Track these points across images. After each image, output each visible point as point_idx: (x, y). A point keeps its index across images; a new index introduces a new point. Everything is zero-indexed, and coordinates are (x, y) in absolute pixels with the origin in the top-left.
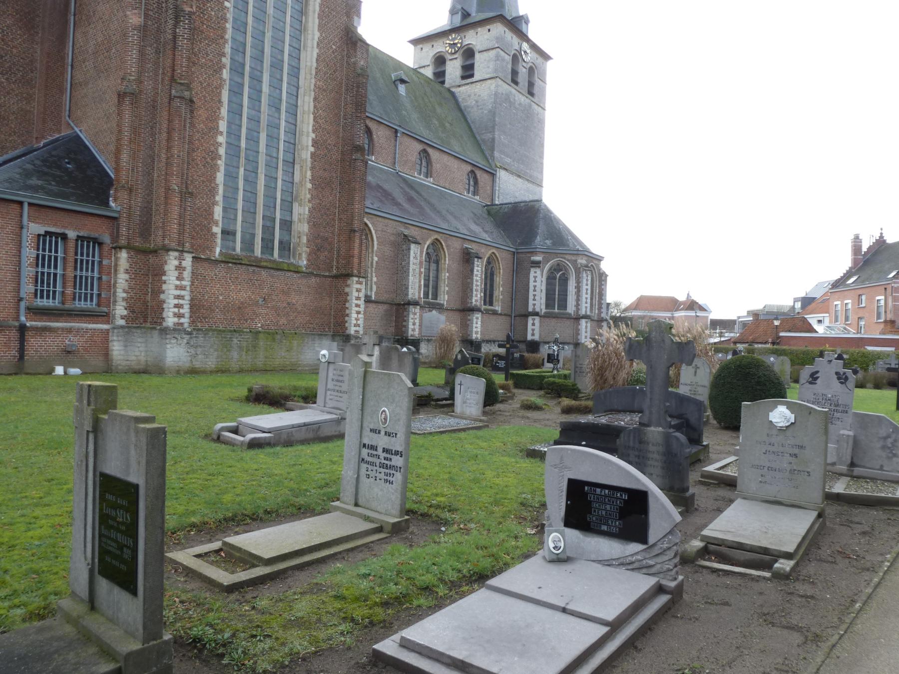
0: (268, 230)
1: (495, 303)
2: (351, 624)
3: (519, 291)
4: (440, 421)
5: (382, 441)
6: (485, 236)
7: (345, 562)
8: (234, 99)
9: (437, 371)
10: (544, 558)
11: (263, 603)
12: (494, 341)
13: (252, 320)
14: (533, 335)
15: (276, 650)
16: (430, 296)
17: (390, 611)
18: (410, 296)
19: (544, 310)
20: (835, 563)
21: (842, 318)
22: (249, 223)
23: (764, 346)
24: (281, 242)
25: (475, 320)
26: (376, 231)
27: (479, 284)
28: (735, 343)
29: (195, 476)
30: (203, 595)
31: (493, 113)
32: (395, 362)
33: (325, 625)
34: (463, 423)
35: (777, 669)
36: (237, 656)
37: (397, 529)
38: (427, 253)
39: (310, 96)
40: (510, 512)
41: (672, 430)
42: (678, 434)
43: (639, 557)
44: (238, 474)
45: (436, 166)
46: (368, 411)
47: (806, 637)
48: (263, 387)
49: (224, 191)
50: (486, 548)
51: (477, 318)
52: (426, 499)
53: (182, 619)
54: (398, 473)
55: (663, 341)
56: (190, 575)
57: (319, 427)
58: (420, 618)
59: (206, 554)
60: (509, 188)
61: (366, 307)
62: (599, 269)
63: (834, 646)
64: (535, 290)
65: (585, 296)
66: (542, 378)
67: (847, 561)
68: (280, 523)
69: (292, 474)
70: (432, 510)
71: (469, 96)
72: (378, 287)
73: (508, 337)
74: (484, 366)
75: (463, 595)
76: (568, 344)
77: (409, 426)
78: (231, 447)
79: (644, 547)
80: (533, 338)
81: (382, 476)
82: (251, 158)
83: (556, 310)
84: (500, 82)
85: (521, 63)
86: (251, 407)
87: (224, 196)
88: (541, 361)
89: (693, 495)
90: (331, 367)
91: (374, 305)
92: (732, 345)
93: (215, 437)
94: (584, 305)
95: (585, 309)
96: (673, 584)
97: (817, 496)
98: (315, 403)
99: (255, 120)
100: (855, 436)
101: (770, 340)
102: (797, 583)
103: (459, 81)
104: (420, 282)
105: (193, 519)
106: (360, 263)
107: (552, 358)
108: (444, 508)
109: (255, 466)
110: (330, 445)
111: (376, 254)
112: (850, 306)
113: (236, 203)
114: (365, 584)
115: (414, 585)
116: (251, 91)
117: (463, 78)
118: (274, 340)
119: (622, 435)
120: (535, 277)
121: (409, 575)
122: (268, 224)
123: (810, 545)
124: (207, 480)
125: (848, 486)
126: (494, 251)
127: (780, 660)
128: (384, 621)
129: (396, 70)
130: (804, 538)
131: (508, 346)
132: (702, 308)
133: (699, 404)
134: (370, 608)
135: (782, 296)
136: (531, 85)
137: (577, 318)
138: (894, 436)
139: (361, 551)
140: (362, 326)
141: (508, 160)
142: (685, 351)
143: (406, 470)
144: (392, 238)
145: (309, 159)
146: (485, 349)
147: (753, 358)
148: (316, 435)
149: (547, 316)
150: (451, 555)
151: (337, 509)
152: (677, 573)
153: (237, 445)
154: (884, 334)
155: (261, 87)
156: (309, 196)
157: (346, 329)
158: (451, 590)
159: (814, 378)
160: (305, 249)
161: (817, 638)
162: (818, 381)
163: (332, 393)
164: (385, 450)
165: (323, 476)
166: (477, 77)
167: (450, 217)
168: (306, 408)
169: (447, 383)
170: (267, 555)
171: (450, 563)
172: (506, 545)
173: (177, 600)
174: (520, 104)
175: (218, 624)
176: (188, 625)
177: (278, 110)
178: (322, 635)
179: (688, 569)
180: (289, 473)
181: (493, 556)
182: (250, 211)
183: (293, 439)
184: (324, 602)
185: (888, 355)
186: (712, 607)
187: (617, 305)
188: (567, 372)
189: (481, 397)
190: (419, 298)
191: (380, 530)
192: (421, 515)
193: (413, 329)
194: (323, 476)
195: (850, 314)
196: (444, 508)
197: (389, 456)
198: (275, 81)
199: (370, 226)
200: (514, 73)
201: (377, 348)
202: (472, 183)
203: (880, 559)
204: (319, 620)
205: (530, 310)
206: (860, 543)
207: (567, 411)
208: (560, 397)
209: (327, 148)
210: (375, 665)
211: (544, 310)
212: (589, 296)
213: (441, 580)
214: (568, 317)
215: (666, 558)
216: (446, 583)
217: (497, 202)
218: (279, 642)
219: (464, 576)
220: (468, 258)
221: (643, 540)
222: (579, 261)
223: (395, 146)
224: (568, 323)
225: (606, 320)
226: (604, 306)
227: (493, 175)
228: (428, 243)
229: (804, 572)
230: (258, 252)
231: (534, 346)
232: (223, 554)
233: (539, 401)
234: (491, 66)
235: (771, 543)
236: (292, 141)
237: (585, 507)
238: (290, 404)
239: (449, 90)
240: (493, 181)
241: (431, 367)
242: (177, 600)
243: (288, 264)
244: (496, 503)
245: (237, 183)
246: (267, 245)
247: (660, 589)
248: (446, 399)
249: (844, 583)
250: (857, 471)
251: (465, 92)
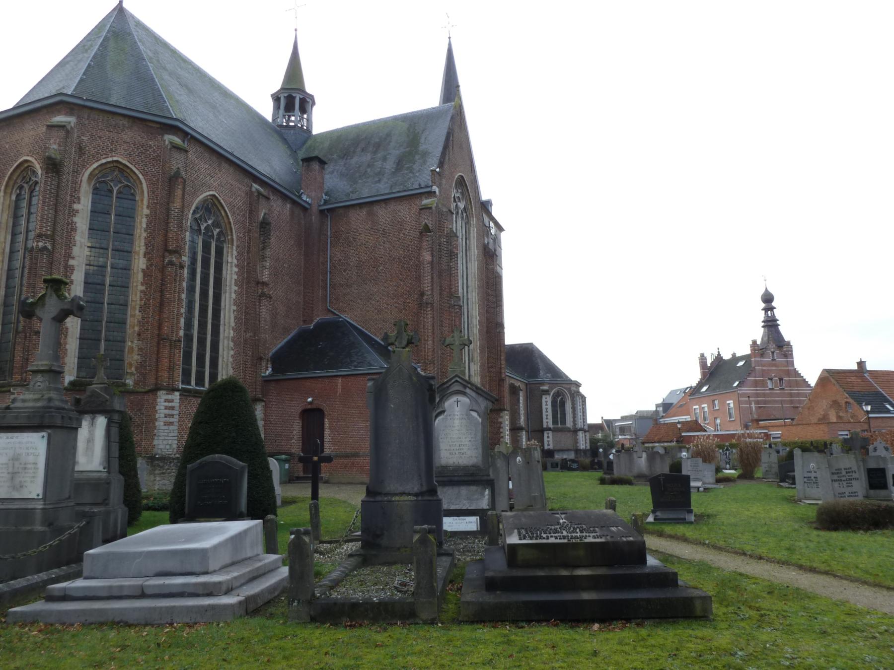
23: (669, 444)
137: (575, 431)
195: (707, 415)
205: (545, 426)
214: (568, 430)
224: (569, 435)
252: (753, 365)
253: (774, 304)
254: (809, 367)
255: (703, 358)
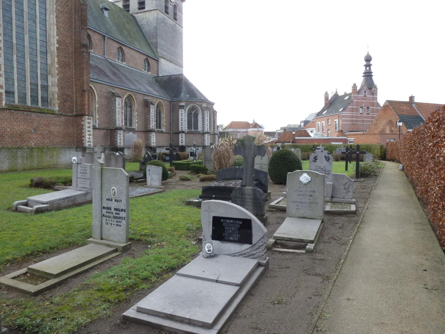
0: (34, 91)
1: (162, 127)
2: (108, 303)
3: (174, 121)
4: (140, 190)
5: (113, 205)
6: (155, 93)
7: (99, 270)
8: (6, 14)
9: (134, 164)
10: (203, 256)
11: (57, 299)
12: (163, 147)
13: (29, 141)
14: (182, 143)
15: (69, 324)
16: (128, 125)
17: (128, 293)
18: (117, 125)
19: (187, 130)
20: (330, 242)
21: (321, 130)
22: (22, 87)
24: (42, 98)
25: (152, 136)
26: (96, 91)
27: (153, 118)
28: (276, 143)
29: (5, 232)
30: (20, 300)
31: (156, 28)
32: (113, 161)
33: (94, 306)
34: (152, 190)
35: (313, 295)
36: (46, 332)
37: (125, 249)
38: (125, 102)
39: (53, 15)
40: (182, 234)
41: (256, 188)
42: (259, 189)
43: (248, 251)
44: (32, 229)
45: (127, 56)
46: (104, 189)
47: (323, 278)
48: (40, 178)
49: (5, 68)
50: (173, 254)
51: (153, 135)
52: (139, 232)
53: (9, 315)
54: (124, 221)
55: (251, 145)
56: (10, 289)
57: (75, 199)
58: (145, 295)
59: (18, 276)
60: (166, 68)
61: (94, 132)
62: (213, 109)
63: (335, 281)
64: (182, 120)
65: (207, 123)
66: (189, 164)
67: (335, 241)
68: (60, 253)
69: (63, 226)
70: (142, 237)
71: (143, 19)
72: (99, 121)
73: (171, 144)
74: (158, 160)
75: (165, 280)
76: (200, 146)
77: (128, 195)
78: (24, 214)
79: (251, 245)
80: (182, 144)
81: (115, 223)
82: (20, 50)
83: (193, 130)
84: (159, 12)
85: (169, 3)
86: (33, 190)
87: (5, 71)
88: (187, 156)
89: (267, 217)
90: (79, 166)
91: (98, 131)
92: (274, 144)
93: (14, 209)
94: (206, 127)
95: (207, 129)
96: (265, 262)
97: (321, 213)
98: (71, 185)
99: (20, 27)
100: (333, 185)
101: (291, 141)
102: (316, 254)
103: (137, 11)
104: (122, 117)
105: (7, 258)
106: (89, 108)
107: (192, 154)
108: (148, 236)
109: (41, 224)
110: (82, 208)
111: (97, 103)
112: (324, 124)
113: (13, 75)
114: (113, 281)
115: (139, 278)
116: (17, 10)
117: (139, 9)
118: (42, 152)
119: (233, 191)
120: (182, 114)
121: (135, 273)
122: (34, 87)
123: (320, 236)
124: (13, 234)
125: (331, 207)
126: (160, 100)
127: (314, 290)
128: (126, 299)
129: (102, 3)
130: (317, 233)
131: (171, 149)
132: (260, 127)
133: (265, 173)
134: (118, 293)
135: (295, 121)
136: (175, 14)
137: (203, 134)
138: (348, 183)
139: (107, 263)
140: (92, 142)
141: (165, 53)
142: (261, 150)
143: (127, 219)
144: (106, 94)
145: (56, 51)
146: (158, 151)
147: (285, 150)
148: (73, 203)
149: (188, 133)
150: (156, 260)
151: (91, 242)
152: (266, 256)
153: (28, 212)
154: (338, 136)
155: (23, 8)
156: (57, 72)
157: (84, 144)
158: (158, 278)
159: (315, 159)
160: (57, 101)
161: (328, 278)
162: (317, 161)
163: (81, 180)
164: (115, 209)
165: (81, 225)
166: (147, 8)
167: (136, 83)
168: (67, 189)
169: (141, 170)
170: (55, 273)
171: (156, 264)
172: (183, 251)
173: (4, 305)
174: (170, 24)
175: (32, 315)
176: (14, 319)
177: (35, 22)
178: (93, 312)
179: (269, 253)
180: (61, 225)
181: (177, 257)
182: (22, 80)
183: (60, 206)
184: (91, 294)
185: (340, 146)
186: (282, 270)
187: (221, 126)
188: (200, 161)
189: (160, 177)
190: (122, 126)
191: (116, 251)
192: (137, 240)
193: (120, 142)
194: (81, 225)
195: (324, 128)
196: (148, 236)
197: (118, 212)
198: (31, 5)
199: (93, 88)
200: (166, 8)
201: (103, 154)
202: (147, 65)
203: (348, 238)
204: (91, 304)
205: (180, 130)
206: (339, 233)
207: (203, 180)
208: (198, 173)
209: (66, 45)
210: (125, 323)
211: (187, 130)
212: (208, 123)
213: (153, 273)
214: (199, 133)
215: (261, 250)
216: (155, 274)
217: (160, 75)
218: (70, 320)
219: (164, 270)
220: (147, 104)
221: (249, 241)
222: (203, 105)
223: (104, 44)
225: (217, 134)
226: (216, 127)
227: (157, 61)
228: (125, 97)
229: (319, 248)
230: (29, 103)
231: (183, 148)
232: (28, 275)
233: (189, 176)
234: (154, 4)
235: (304, 237)
236: (45, 40)
237: (222, 229)
238: (56, 187)
239: (132, 15)
240: (158, 64)
241: (131, 162)
242: (4, 305)
243: (48, 110)
244: (175, 230)
245: (13, 64)
246: (34, 99)
247: (259, 265)
248: (141, 178)
249: (335, 251)
250: (334, 200)
251: (140, 16)
252: (352, 99)
253: (371, 63)
254: (382, 99)
255: (326, 95)
